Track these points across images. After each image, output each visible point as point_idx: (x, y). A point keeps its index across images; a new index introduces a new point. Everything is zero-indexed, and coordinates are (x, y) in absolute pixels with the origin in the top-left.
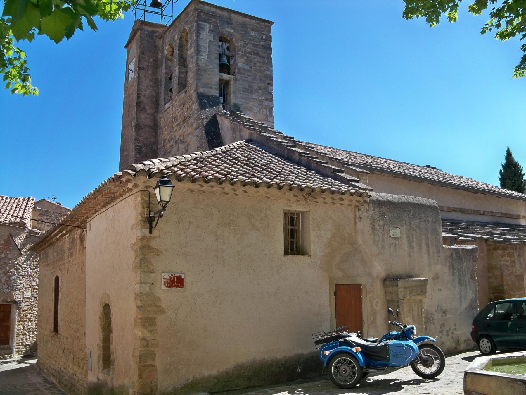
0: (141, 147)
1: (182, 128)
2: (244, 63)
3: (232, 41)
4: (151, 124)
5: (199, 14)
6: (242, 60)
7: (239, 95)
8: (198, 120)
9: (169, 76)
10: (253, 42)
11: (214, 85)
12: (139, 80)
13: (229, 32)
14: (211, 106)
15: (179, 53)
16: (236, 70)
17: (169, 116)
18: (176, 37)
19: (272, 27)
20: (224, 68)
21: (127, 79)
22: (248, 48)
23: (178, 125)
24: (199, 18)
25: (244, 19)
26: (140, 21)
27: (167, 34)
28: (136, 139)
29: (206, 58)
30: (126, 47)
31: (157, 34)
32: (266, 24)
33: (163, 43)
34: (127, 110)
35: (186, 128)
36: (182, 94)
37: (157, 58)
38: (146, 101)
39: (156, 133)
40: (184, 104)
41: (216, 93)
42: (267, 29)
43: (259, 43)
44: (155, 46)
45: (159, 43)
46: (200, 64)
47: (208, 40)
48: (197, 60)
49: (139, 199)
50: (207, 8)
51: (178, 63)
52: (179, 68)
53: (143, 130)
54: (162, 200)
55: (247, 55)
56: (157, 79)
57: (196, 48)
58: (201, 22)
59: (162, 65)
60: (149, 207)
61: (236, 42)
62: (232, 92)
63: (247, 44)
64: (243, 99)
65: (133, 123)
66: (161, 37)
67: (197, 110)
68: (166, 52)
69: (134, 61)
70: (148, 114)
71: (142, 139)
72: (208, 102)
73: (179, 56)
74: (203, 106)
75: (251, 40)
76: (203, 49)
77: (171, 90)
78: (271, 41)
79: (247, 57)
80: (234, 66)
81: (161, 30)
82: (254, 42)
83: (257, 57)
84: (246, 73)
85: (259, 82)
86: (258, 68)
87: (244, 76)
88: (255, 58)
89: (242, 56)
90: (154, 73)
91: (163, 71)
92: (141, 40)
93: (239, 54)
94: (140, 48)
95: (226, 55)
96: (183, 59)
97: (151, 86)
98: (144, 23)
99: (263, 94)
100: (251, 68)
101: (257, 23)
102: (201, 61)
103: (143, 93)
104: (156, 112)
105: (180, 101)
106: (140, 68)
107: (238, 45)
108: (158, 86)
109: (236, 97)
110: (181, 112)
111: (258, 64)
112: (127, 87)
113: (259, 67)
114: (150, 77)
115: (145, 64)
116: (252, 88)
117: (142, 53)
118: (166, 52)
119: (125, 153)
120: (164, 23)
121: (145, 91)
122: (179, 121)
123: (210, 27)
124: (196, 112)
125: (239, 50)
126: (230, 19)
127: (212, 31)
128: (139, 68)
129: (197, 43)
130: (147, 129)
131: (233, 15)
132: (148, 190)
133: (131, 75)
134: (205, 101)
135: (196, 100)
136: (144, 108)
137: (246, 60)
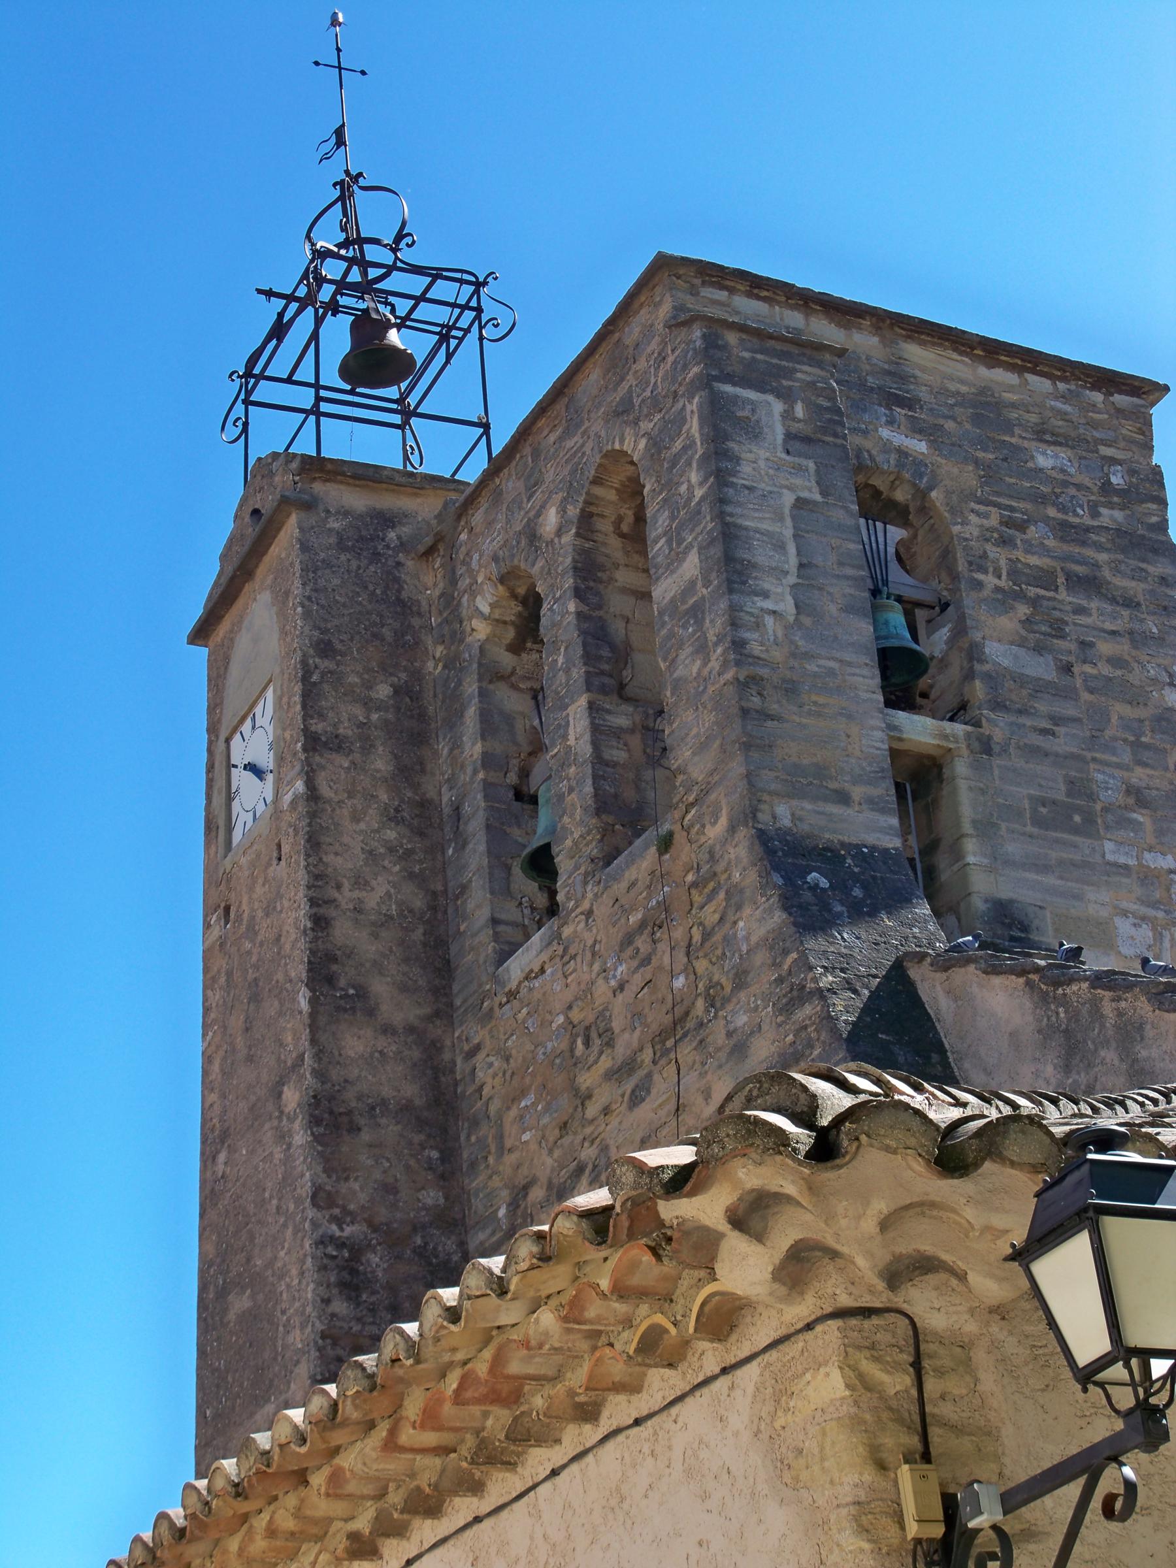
0: (356, 1251)
1: (662, 1087)
2: (1022, 643)
3: (925, 509)
4: (411, 1091)
5: (712, 343)
6: (1008, 623)
7: (1013, 848)
8: (787, 1008)
9: (512, 778)
10: (1052, 512)
11: (856, 780)
12: (313, 815)
13: (902, 453)
14: (863, 912)
15: (579, 614)
16: (979, 690)
17: (545, 1024)
18: (551, 518)
19: (1159, 413)
20: (903, 678)
21: (217, 826)
22: (1029, 549)
23: (616, 1074)
24: (716, 365)
25: (983, 371)
26: (288, 456)
27: (478, 517)
28: (321, 1198)
29: (787, 606)
30: (201, 633)
31: (406, 530)
32: (1120, 399)
33: (453, 582)
34: (236, 1022)
35: (690, 1080)
36: (641, 862)
37: (417, 675)
38: (369, 948)
39: (449, 1155)
40: (654, 924)
41: (875, 827)
42: (1128, 428)
43: (1095, 514)
44: (399, 601)
45: (425, 583)
46: (755, 648)
47: (788, 499)
48: (734, 624)
49: (828, 1386)
50: (749, 308)
51: (578, 673)
52: (591, 706)
53: (365, 1136)
54: (1136, 1337)
55: (1032, 591)
56: (425, 806)
57: (716, 551)
58: (728, 388)
59: (454, 718)
60: (926, 1457)
61: (952, 511)
62: (967, 828)
63: (1022, 527)
64: (1045, 869)
65: (292, 1097)
66: (437, 546)
67: (776, 945)
68: (481, 630)
69: (265, 711)
70: (387, 1030)
71: (363, 1197)
72: (841, 885)
73: (583, 633)
74: (810, 916)
75: (1041, 499)
76: (762, 555)
77: (542, 864)
78: (1163, 503)
79: (1035, 602)
80: (954, 671)
81: (426, 507)
82: (1063, 509)
83: (1094, 604)
84: (1042, 707)
85: (1126, 757)
86: (1106, 670)
87: (1028, 722)
88: (1080, 610)
89: (1004, 600)
90: (409, 772)
91: (463, 759)
92: (311, 570)
93: (979, 585)
94: (307, 615)
95: (899, 599)
96: (613, 647)
97: (391, 850)
98: (317, 467)
99: (1160, 833)
100: (1067, 669)
101: (1063, 397)
102: (758, 626)
103: (346, 896)
104: (437, 1014)
105: (626, 911)
106: (314, 744)
107: (971, 527)
108: (435, 850)
109: (998, 862)
110: (638, 980)
111: (1105, 648)
112: (228, 877)
113: (1116, 662)
114: (384, 797)
115: (344, 716)
116: (1092, 797)
117: (325, 648)
118: (481, 630)
119: (240, 1303)
120: (437, 464)
121: (360, 882)
122: (626, 1042)
123: (788, 415)
124: (761, 957)
125: (980, 563)
126: (897, 372)
127: (807, 440)
128: (313, 743)
129: (721, 515)
130: (391, 1130)
131: (916, 353)
132: (898, 1301)
133: (252, 796)
134: (816, 883)
135: (753, 877)
136: (362, 993)
137: (1027, 622)
